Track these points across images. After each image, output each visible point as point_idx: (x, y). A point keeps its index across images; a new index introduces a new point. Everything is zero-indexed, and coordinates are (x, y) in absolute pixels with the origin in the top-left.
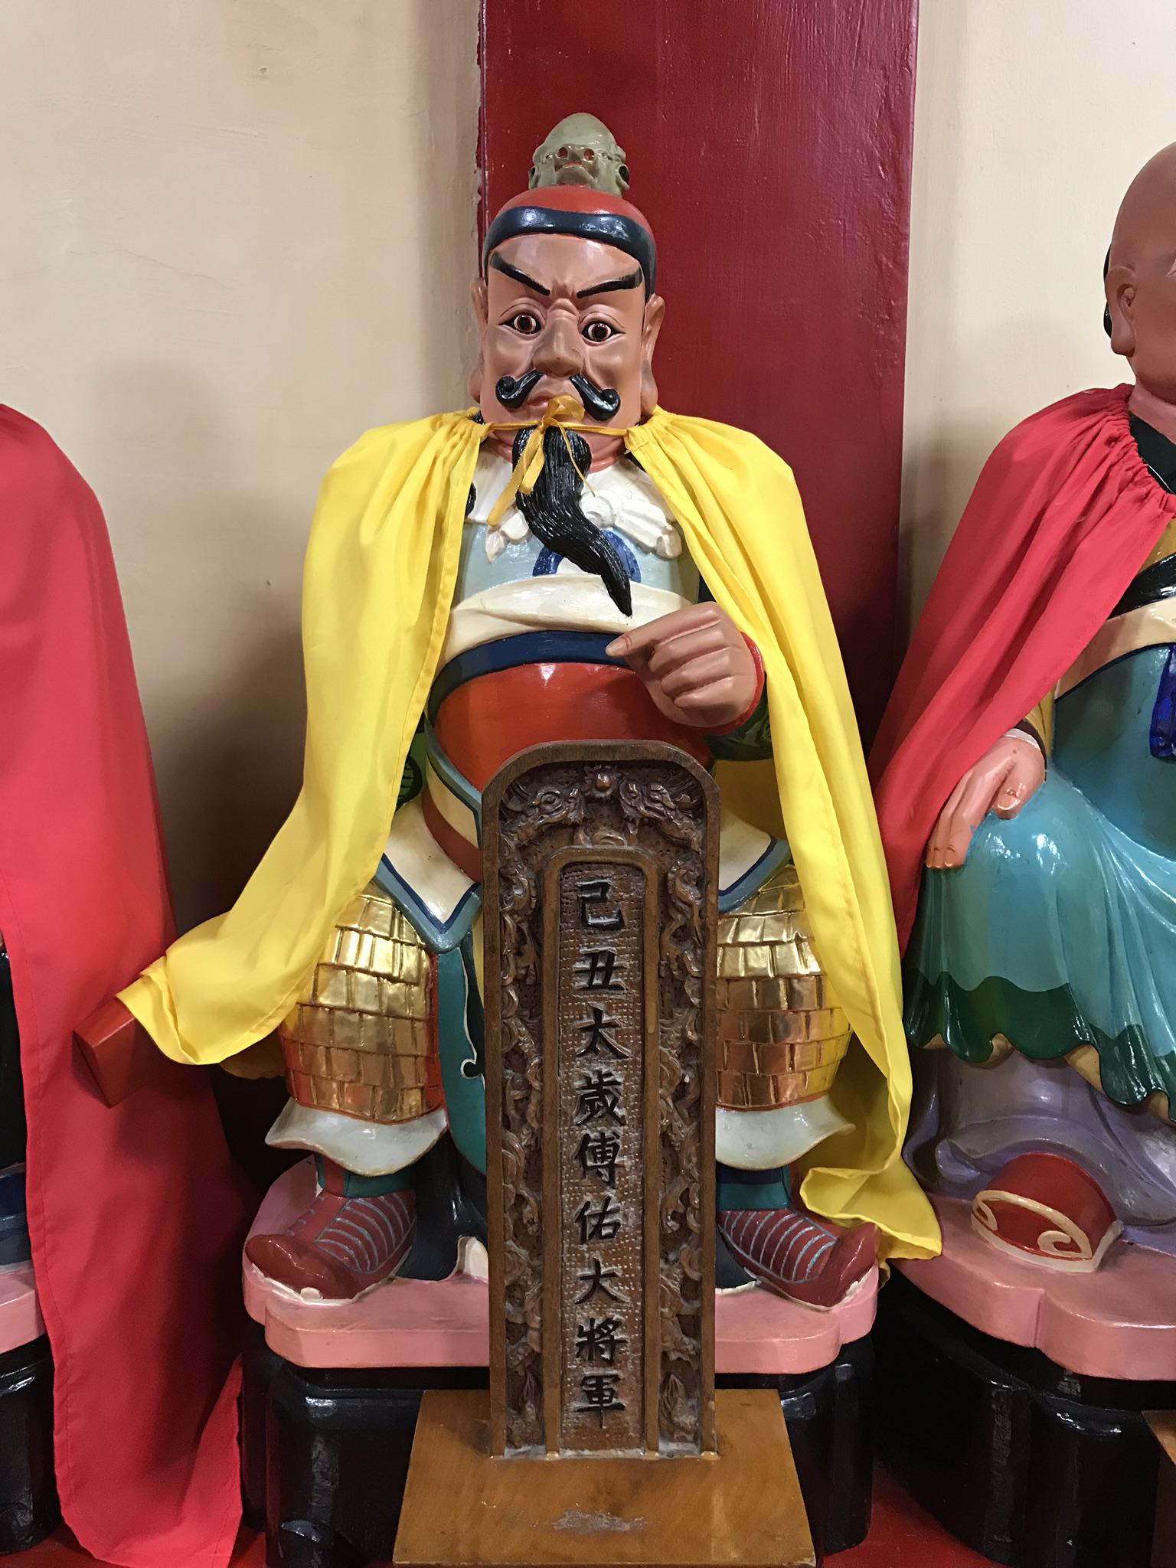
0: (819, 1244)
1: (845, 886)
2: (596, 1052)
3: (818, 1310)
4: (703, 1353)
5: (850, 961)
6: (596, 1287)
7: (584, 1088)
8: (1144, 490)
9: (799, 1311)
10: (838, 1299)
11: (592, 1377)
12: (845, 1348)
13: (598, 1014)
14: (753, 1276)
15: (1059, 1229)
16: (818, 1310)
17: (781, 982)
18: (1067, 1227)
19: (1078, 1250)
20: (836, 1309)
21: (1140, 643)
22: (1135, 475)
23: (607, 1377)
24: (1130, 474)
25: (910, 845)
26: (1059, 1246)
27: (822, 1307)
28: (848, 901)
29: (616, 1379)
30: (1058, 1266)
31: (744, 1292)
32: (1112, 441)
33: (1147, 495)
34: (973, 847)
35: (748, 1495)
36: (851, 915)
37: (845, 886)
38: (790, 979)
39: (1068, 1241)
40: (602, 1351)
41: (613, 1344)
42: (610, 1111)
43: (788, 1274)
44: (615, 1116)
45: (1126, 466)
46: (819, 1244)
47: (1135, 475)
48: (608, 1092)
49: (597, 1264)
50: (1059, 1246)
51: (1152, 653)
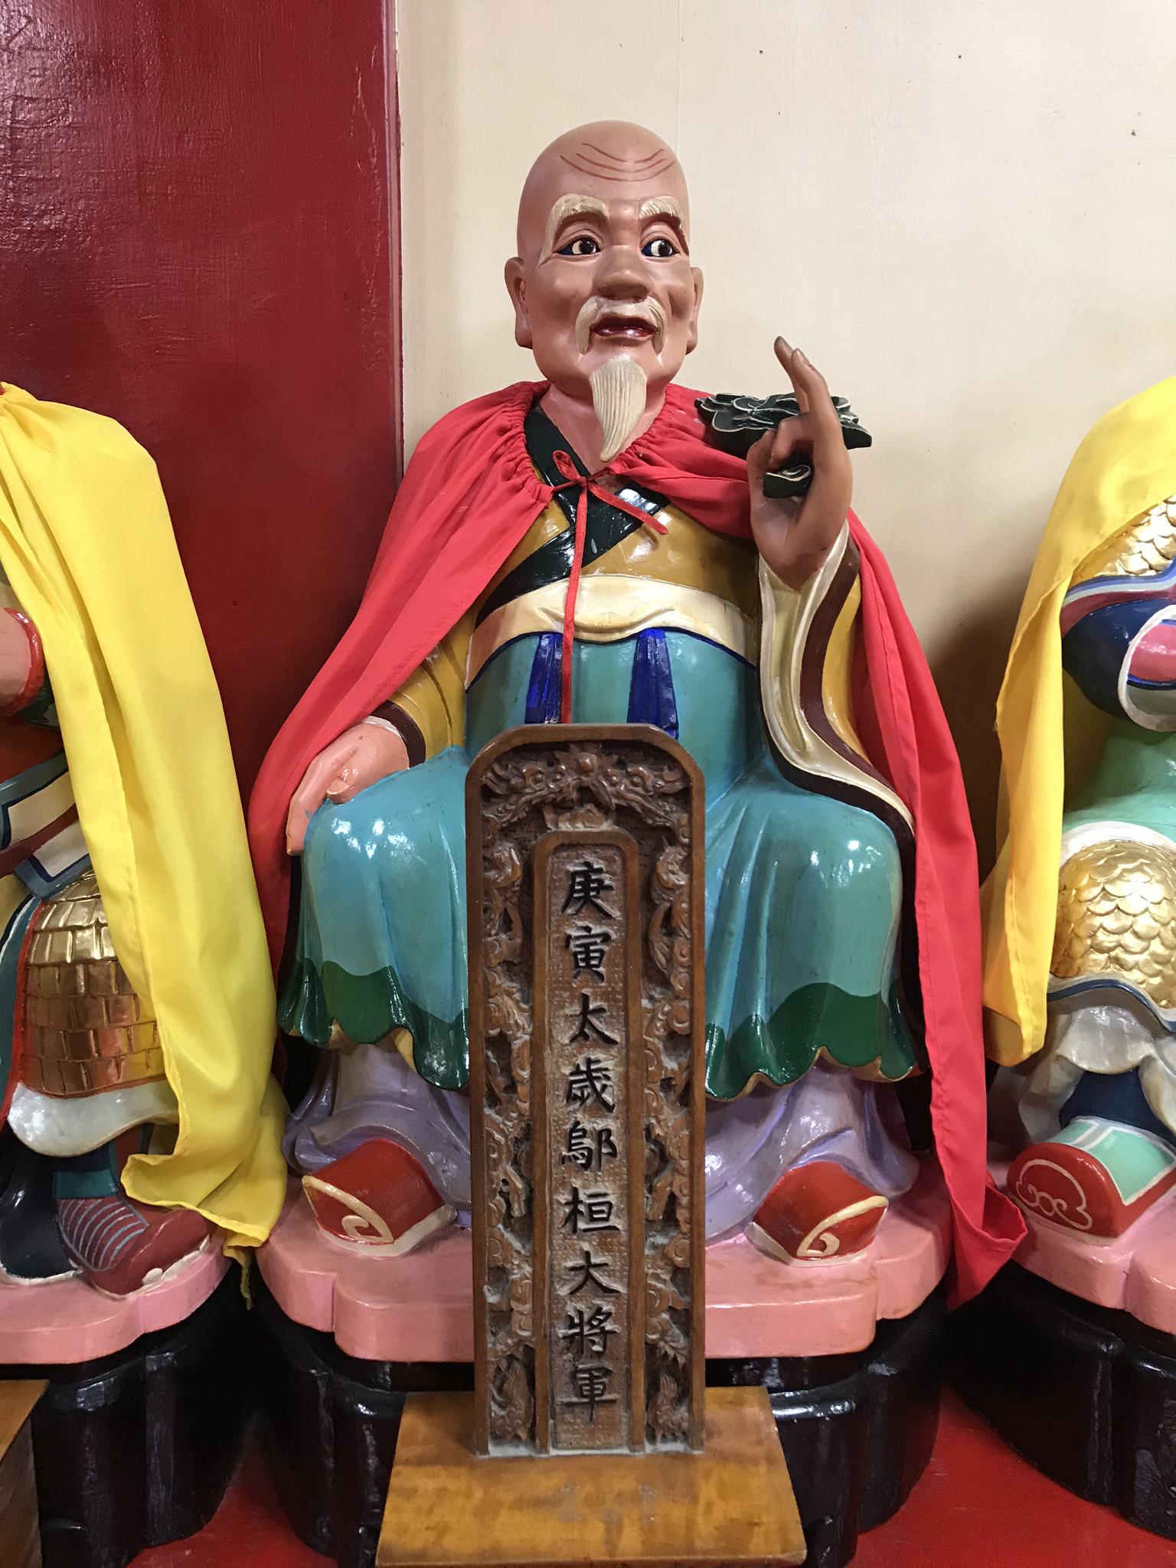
0: (134, 1229)
1: (128, 870)
2: (586, 1037)
3: (114, 1299)
4: (689, 1320)
5: (130, 944)
6: (585, 1022)
7: (572, 1074)
8: (524, 477)
9: (102, 1299)
10: (137, 1285)
11: (583, 1371)
12: (883, 1327)
13: (588, 1254)
14: (74, 1265)
15: (354, 1213)
16: (114, 1299)
17: (80, 969)
18: (360, 1211)
19: (378, 1234)
20: (132, 1297)
21: (515, 632)
22: (517, 465)
23: (598, 1369)
24: (512, 464)
25: (265, 827)
26: (361, 1230)
27: (116, 1296)
28: (130, 885)
29: (607, 1372)
30: (362, 1249)
31: (60, 1281)
32: (502, 431)
33: (523, 484)
34: (310, 832)
35: (745, 1487)
36: (132, 899)
37: (128, 870)
38: (89, 962)
39: (366, 1225)
40: (594, 1343)
41: (604, 1333)
42: (598, 1095)
43: (96, 1264)
44: (605, 1103)
45: (509, 456)
46: (134, 1229)
47: (517, 465)
48: (598, 1078)
49: (588, 1254)
50: (361, 1230)
51: (525, 643)
